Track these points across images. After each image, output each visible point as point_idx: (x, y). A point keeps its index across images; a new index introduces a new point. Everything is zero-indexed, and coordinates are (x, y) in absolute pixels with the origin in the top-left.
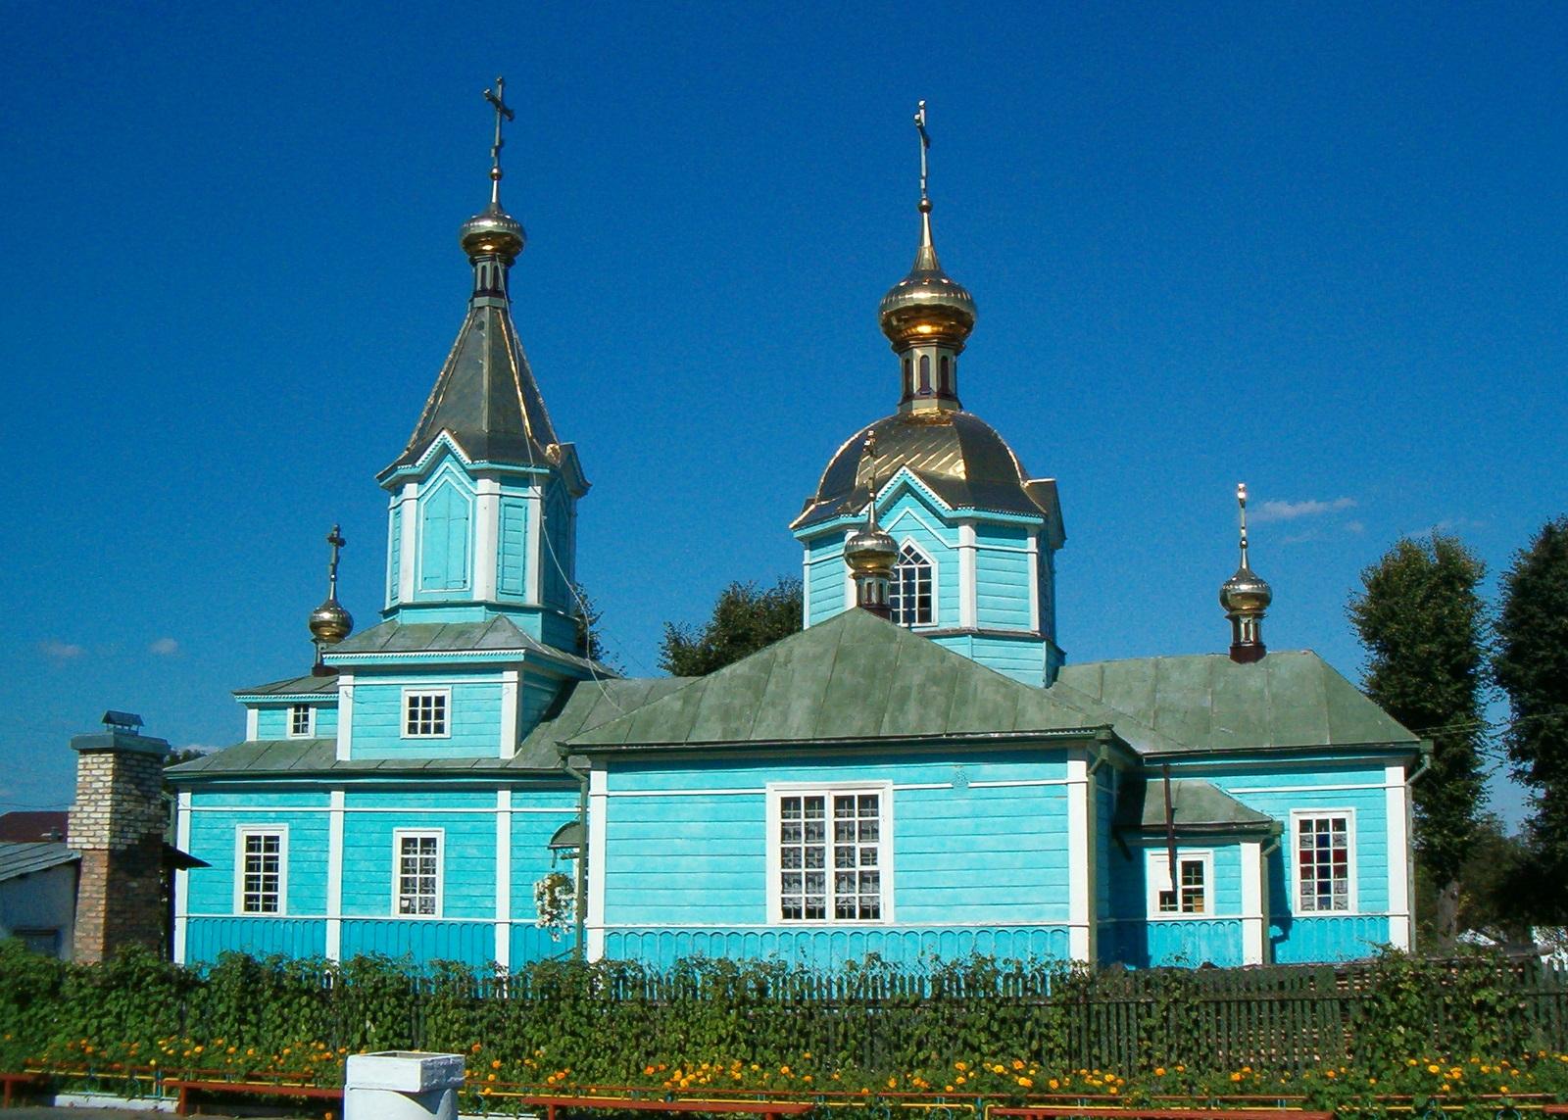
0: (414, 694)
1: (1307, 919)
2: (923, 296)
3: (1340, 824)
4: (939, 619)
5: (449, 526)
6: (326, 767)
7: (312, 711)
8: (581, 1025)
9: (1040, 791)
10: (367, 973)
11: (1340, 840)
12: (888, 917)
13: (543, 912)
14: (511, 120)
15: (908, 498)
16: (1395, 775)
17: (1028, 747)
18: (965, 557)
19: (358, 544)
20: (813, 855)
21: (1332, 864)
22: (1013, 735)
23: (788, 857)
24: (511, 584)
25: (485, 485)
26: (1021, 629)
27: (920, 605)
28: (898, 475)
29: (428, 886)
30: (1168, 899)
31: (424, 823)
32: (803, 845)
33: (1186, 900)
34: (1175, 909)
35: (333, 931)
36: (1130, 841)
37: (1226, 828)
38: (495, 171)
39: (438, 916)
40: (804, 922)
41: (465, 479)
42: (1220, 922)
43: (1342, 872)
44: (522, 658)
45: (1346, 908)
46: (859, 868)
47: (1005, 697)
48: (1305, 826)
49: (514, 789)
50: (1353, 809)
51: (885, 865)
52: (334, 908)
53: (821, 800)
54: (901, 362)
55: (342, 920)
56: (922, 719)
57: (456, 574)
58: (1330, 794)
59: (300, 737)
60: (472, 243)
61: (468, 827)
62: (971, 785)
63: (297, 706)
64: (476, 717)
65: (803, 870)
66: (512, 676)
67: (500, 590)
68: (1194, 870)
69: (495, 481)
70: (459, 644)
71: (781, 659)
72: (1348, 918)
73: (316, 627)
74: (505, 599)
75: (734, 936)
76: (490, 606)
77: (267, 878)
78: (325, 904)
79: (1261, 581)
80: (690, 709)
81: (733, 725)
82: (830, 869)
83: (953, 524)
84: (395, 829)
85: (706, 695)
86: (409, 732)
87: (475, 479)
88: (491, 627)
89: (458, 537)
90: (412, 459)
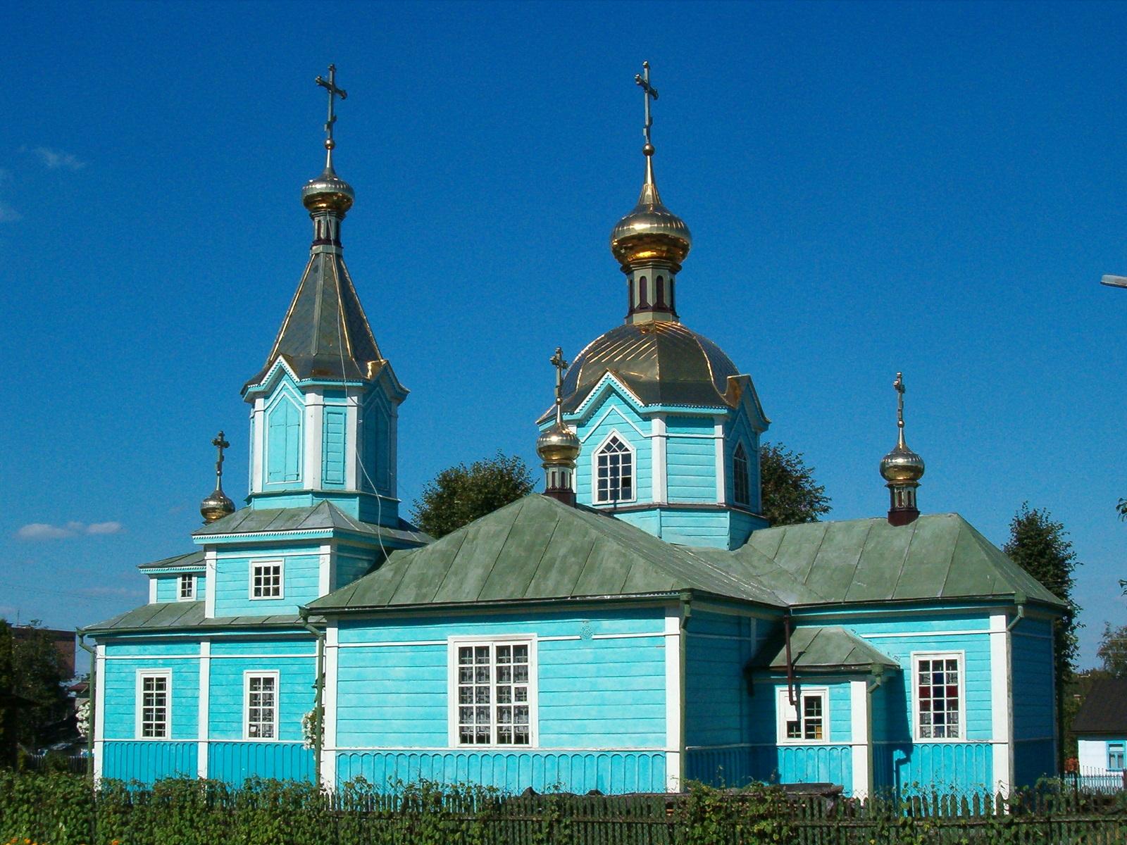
0: (258, 565)
1: (925, 745)
2: (640, 227)
3: (952, 664)
4: (638, 495)
5: (288, 428)
6: (194, 623)
7: (194, 579)
8: (186, 828)
9: (644, 642)
10: (60, 787)
11: (954, 678)
12: (534, 743)
13: (308, 737)
14: (656, 98)
15: (613, 398)
16: (998, 623)
17: (633, 606)
18: (657, 444)
19: (229, 446)
20: (483, 693)
21: (945, 699)
22: (621, 596)
23: (464, 695)
24: (333, 475)
25: (311, 398)
26: (709, 502)
27: (623, 485)
28: (603, 379)
29: (269, 715)
30: (793, 727)
31: (266, 666)
32: (474, 685)
33: (808, 729)
34: (799, 736)
35: (203, 750)
36: (758, 680)
37: (837, 669)
38: (328, 142)
39: (275, 739)
40: (475, 746)
41: (297, 393)
42: (834, 747)
43: (954, 705)
44: (331, 535)
45: (957, 737)
46: (514, 703)
47: (622, 566)
48: (924, 665)
49: (213, 640)
50: (963, 651)
51: (532, 701)
52: (203, 735)
53: (487, 648)
54: (628, 282)
55: (209, 742)
56: (558, 583)
57: (292, 468)
58: (946, 639)
59: (187, 599)
60: (310, 201)
61: (295, 668)
62: (594, 637)
63: (184, 576)
64: (303, 582)
65: (474, 705)
66: (326, 549)
67: (325, 480)
68: (813, 704)
69: (319, 395)
70: (288, 525)
71: (470, 536)
72: (958, 745)
73: (205, 512)
74: (328, 488)
75: (436, 757)
76: (316, 494)
77: (158, 710)
78: (197, 729)
79: (913, 456)
80: (398, 578)
81: (424, 591)
82: (493, 705)
83: (647, 417)
84: (245, 671)
85: (412, 566)
86: (256, 595)
87: (304, 394)
88: (314, 511)
89: (299, 439)
90: (258, 380)
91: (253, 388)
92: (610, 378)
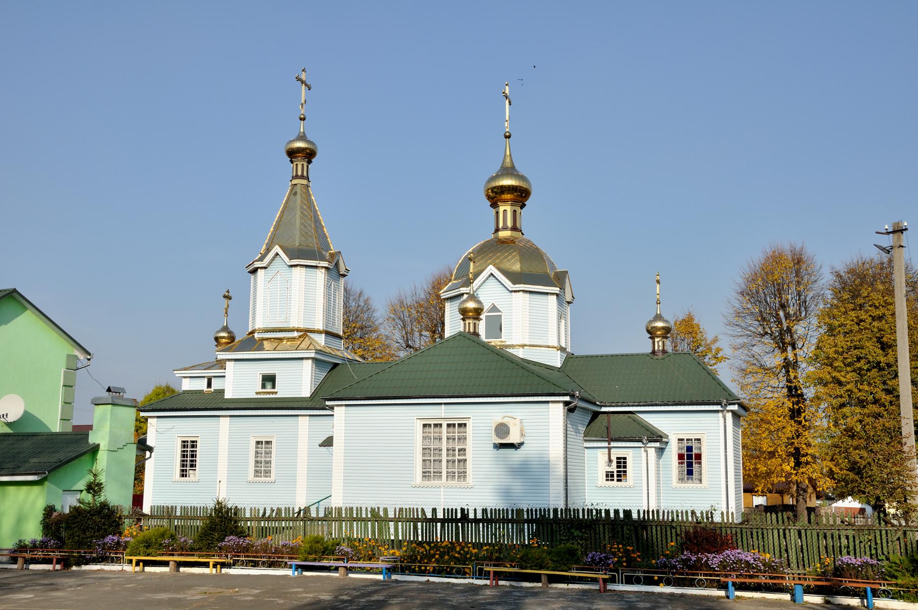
68: (622, 462)
77: (192, 461)
90: (261, 259)
91: (257, 264)
92: (491, 269)
